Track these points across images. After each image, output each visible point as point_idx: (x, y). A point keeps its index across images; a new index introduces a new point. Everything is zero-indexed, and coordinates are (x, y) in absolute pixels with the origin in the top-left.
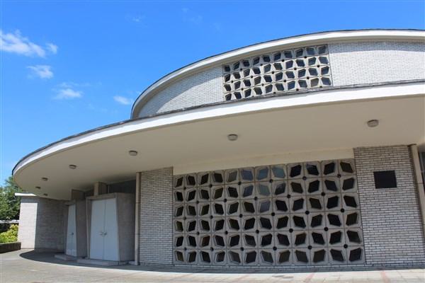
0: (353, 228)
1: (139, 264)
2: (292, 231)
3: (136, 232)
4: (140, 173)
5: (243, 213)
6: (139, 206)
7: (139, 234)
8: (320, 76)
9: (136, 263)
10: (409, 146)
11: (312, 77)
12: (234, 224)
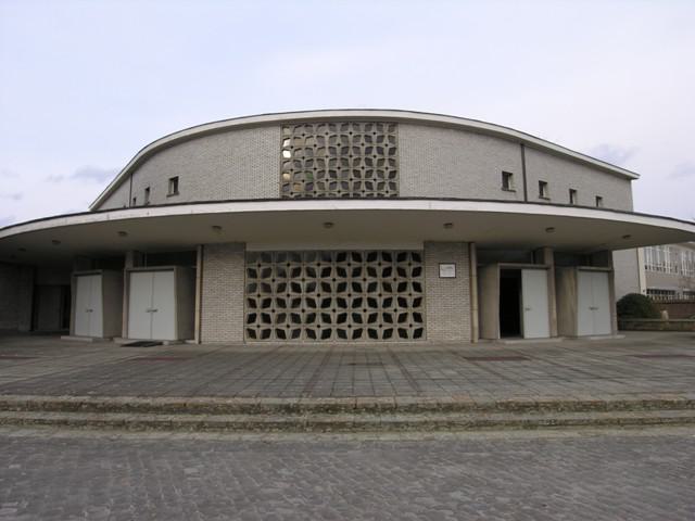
0: (417, 310)
2: (365, 311)
3: (197, 308)
4: (203, 246)
5: (261, 294)
8: (386, 156)
9: (196, 341)
10: (470, 243)
11: (379, 157)
12: (311, 303)
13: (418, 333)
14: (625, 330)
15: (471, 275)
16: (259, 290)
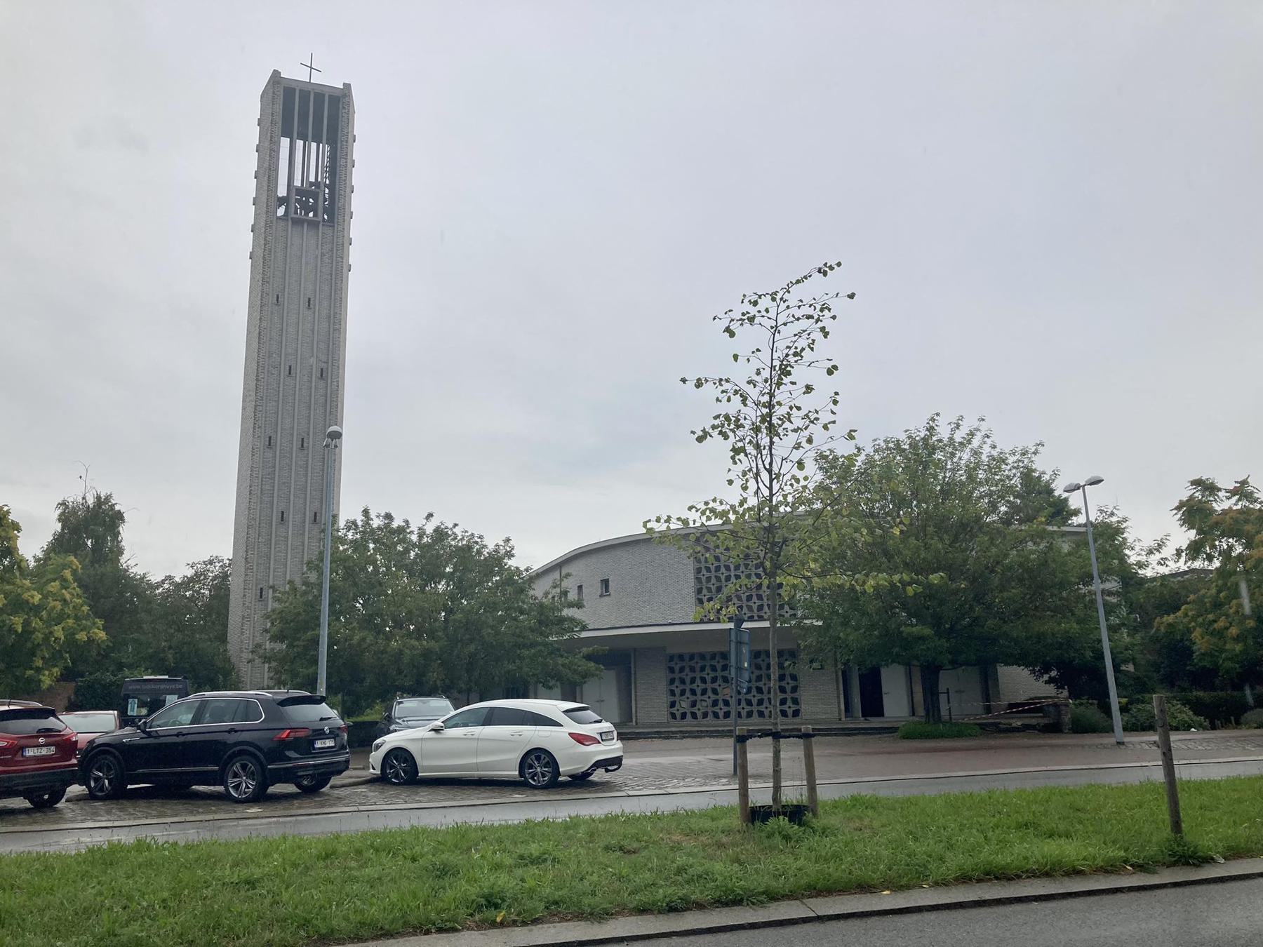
0: (795, 695)
1: (637, 723)
6: (635, 678)
7: (636, 700)
9: (634, 723)
13: (796, 713)
14: (292, 88)
15: (838, 684)
16: (677, 683)
